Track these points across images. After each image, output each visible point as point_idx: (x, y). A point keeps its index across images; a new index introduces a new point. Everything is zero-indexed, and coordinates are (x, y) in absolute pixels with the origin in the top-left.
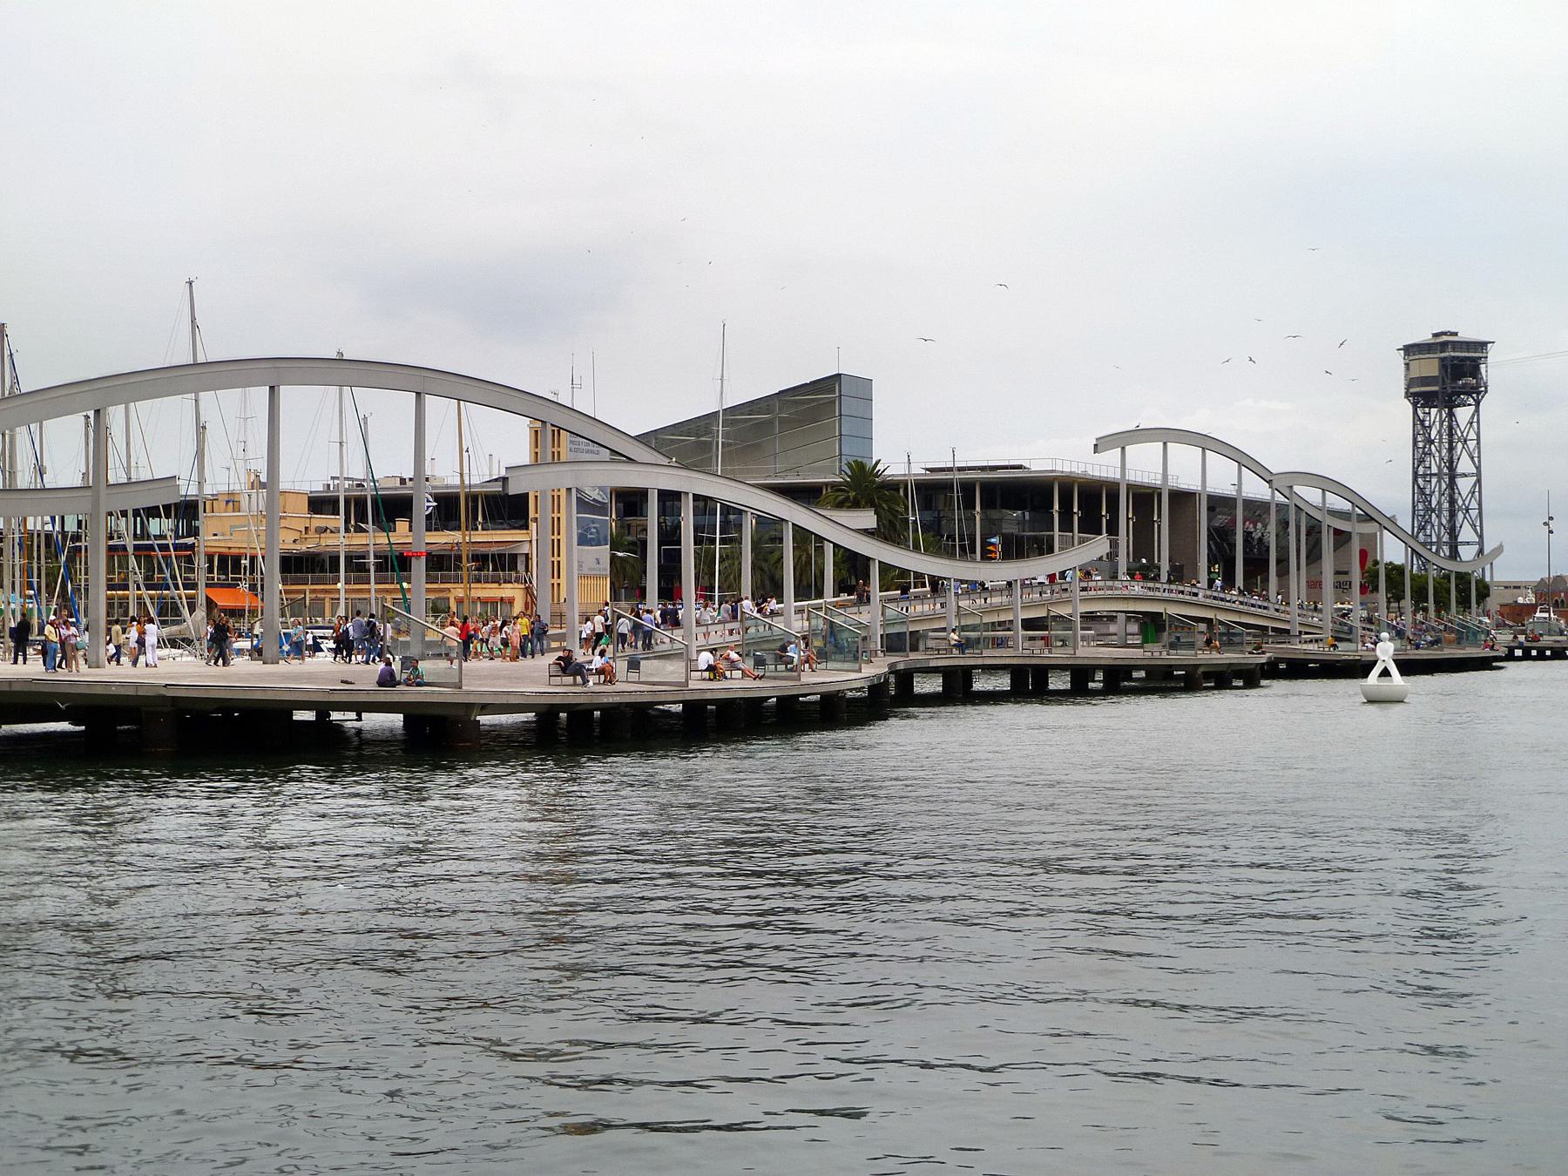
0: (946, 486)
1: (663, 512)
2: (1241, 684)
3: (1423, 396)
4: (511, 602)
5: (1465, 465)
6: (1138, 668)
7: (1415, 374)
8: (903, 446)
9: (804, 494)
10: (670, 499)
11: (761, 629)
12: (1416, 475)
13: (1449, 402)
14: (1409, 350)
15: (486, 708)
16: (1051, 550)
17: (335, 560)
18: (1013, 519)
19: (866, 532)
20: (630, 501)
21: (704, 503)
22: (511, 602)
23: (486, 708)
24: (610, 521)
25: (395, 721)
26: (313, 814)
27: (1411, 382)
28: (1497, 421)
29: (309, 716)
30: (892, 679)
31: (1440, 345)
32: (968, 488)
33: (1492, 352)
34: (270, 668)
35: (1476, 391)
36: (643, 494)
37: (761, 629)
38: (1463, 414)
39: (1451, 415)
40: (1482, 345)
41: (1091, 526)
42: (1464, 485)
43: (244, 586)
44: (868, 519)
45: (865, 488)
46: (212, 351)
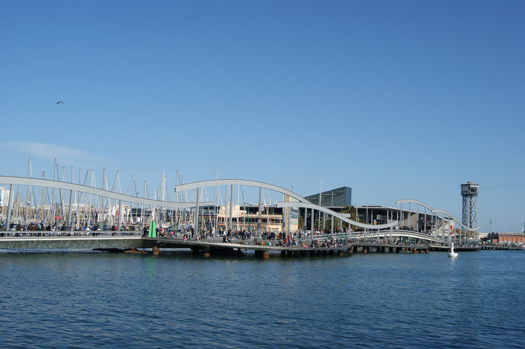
0: (365, 210)
1: (308, 213)
2: (235, 249)
3: (465, 195)
4: (278, 229)
6: (360, 246)
7: (463, 190)
8: (357, 202)
9: (337, 210)
10: (309, 210)
12: (463, 211)
14: (462, 185)
16: (386, 223)
17: (267, 219)
18: (379, 217)
19: (350, 218)
20: (302, 210)
21: (316, 211)
22: (278, 229)
24: (297, 214)
25: (253, 251)
26: (231, 266)
27: (462, 192)
28: (478, 202)
29: (236, 249)
30: (353, 248)
32: (370, 210)
36: (304, 208)
41: (395, 218)
44: (349, 215)
45: (350, 210)
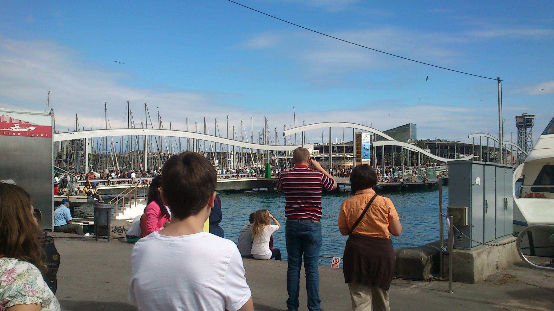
3: (519, 126)
5: (529, 140)
7: (518, 122)
11: (222, 125)
13: (526, 127)
14: (516, 117)
15: (308, 267)
23: (308, 267)
27: (517, 124)
31: (523, 116)
33: (534, 117)
34: (514, 183)
35: (531, 125)
37: (222, 125)
38: (528, 130)
39: (375, 196)
40: (533, 116)
42: (529, 144)
43: (431, 276)
46: (528, 246)
